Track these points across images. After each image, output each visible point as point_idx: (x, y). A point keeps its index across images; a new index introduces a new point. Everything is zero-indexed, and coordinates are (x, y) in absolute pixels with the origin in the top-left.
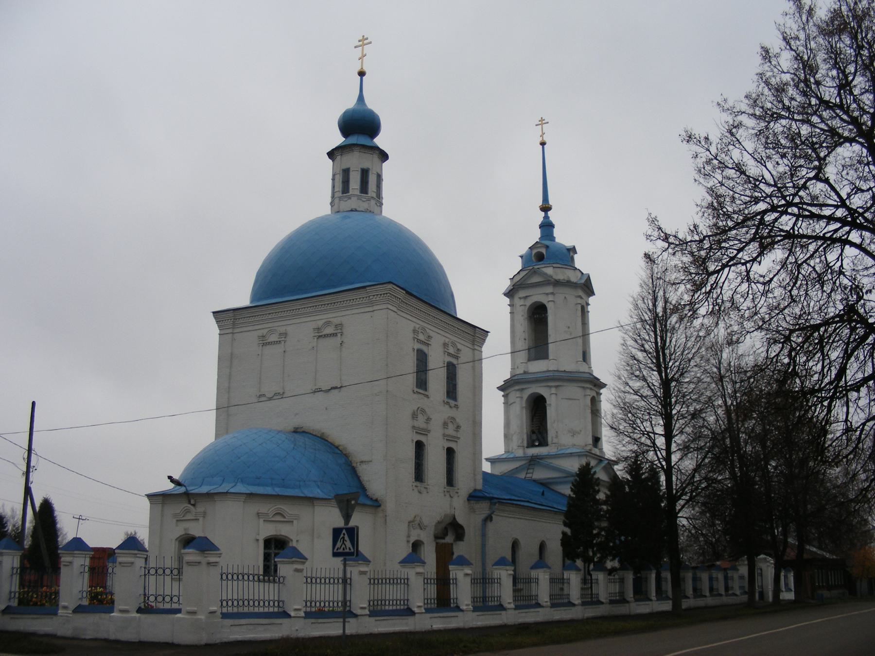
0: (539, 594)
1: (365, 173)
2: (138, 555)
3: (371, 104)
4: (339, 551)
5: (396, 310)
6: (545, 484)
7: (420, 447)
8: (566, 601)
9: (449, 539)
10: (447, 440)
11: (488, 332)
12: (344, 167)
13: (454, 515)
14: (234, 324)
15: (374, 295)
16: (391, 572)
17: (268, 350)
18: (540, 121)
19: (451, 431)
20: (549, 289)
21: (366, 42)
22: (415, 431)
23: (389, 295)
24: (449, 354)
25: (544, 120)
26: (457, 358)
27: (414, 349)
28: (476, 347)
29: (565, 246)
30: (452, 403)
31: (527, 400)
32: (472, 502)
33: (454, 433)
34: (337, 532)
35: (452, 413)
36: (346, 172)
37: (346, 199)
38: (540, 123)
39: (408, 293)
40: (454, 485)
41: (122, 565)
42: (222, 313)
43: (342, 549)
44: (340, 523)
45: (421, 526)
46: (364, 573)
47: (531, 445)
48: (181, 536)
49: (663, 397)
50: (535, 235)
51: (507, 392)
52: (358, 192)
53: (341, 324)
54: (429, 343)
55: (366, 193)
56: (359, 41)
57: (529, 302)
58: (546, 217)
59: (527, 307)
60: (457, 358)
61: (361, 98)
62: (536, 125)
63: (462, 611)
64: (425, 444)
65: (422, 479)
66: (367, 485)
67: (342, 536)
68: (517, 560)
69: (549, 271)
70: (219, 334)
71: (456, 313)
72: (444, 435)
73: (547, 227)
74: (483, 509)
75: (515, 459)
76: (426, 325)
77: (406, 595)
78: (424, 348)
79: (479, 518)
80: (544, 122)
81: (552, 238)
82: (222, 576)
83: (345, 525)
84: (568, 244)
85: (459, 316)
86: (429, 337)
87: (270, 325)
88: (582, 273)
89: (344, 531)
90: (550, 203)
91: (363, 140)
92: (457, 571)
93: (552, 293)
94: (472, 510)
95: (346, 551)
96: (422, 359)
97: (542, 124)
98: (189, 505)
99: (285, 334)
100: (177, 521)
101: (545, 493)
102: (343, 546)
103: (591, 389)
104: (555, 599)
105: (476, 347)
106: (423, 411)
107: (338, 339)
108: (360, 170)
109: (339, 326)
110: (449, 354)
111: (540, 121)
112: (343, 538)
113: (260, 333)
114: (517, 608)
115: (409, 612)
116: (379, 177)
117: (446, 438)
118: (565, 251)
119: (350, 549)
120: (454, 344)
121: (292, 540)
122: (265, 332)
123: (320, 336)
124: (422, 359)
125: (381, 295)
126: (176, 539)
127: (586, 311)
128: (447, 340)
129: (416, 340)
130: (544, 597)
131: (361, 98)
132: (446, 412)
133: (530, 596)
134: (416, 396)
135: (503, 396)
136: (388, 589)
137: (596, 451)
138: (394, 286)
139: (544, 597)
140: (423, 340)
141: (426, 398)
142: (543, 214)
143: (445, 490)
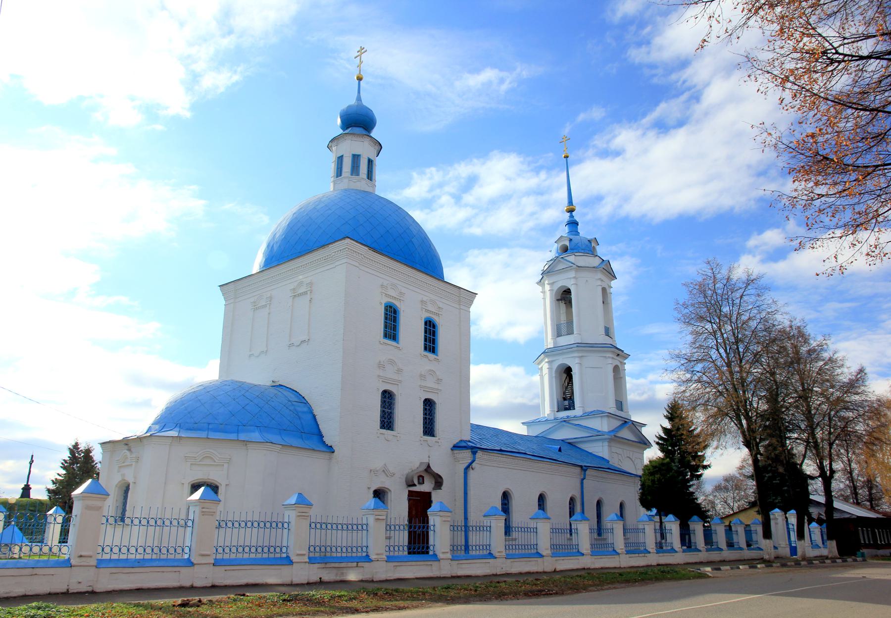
0: (491, 543)
3: (367, 102)
5: (357, 265)
8: (669, 548)
10: (382, 381)
11: (477, 294)
13: (429, 464)
15: (335, 252)
20: (572, 274)
21: (363, 51)
23: (347, 249)
24: (427, 311)
27: (381, 303)
28: (462, 307)
30: (431, 356)
31: (556, 371)
32: (456, 452)
33: (435, 386)
36: (340, 159)
40: (394, 429)
52: (348, 174)
55: (358, 174)
56: (358, 52)
58: (572, 216)
61: (359, 99)
65: (393, 427)
68: (624, 515)
69: (572, 258)
70: (225, 305)
71: (444, 279)
73: (573, 224)
77: (488, 540)
81: (577, 233)
88: (603, 260)
96: (391, 316)
100: (120, 467)
103: (613, 358)
105: (462, 307)
107: (308, 297)
108: (351, 156)
110: (427, 311)
113: (252, 300)
114: (628, 552)
115: (289, 561)
121: (390, 491)
128: (425, 299)
130: (620, 545)
131: (359, 99)
133: (601, 545)
139: (651, 545)
142: (569, 214)
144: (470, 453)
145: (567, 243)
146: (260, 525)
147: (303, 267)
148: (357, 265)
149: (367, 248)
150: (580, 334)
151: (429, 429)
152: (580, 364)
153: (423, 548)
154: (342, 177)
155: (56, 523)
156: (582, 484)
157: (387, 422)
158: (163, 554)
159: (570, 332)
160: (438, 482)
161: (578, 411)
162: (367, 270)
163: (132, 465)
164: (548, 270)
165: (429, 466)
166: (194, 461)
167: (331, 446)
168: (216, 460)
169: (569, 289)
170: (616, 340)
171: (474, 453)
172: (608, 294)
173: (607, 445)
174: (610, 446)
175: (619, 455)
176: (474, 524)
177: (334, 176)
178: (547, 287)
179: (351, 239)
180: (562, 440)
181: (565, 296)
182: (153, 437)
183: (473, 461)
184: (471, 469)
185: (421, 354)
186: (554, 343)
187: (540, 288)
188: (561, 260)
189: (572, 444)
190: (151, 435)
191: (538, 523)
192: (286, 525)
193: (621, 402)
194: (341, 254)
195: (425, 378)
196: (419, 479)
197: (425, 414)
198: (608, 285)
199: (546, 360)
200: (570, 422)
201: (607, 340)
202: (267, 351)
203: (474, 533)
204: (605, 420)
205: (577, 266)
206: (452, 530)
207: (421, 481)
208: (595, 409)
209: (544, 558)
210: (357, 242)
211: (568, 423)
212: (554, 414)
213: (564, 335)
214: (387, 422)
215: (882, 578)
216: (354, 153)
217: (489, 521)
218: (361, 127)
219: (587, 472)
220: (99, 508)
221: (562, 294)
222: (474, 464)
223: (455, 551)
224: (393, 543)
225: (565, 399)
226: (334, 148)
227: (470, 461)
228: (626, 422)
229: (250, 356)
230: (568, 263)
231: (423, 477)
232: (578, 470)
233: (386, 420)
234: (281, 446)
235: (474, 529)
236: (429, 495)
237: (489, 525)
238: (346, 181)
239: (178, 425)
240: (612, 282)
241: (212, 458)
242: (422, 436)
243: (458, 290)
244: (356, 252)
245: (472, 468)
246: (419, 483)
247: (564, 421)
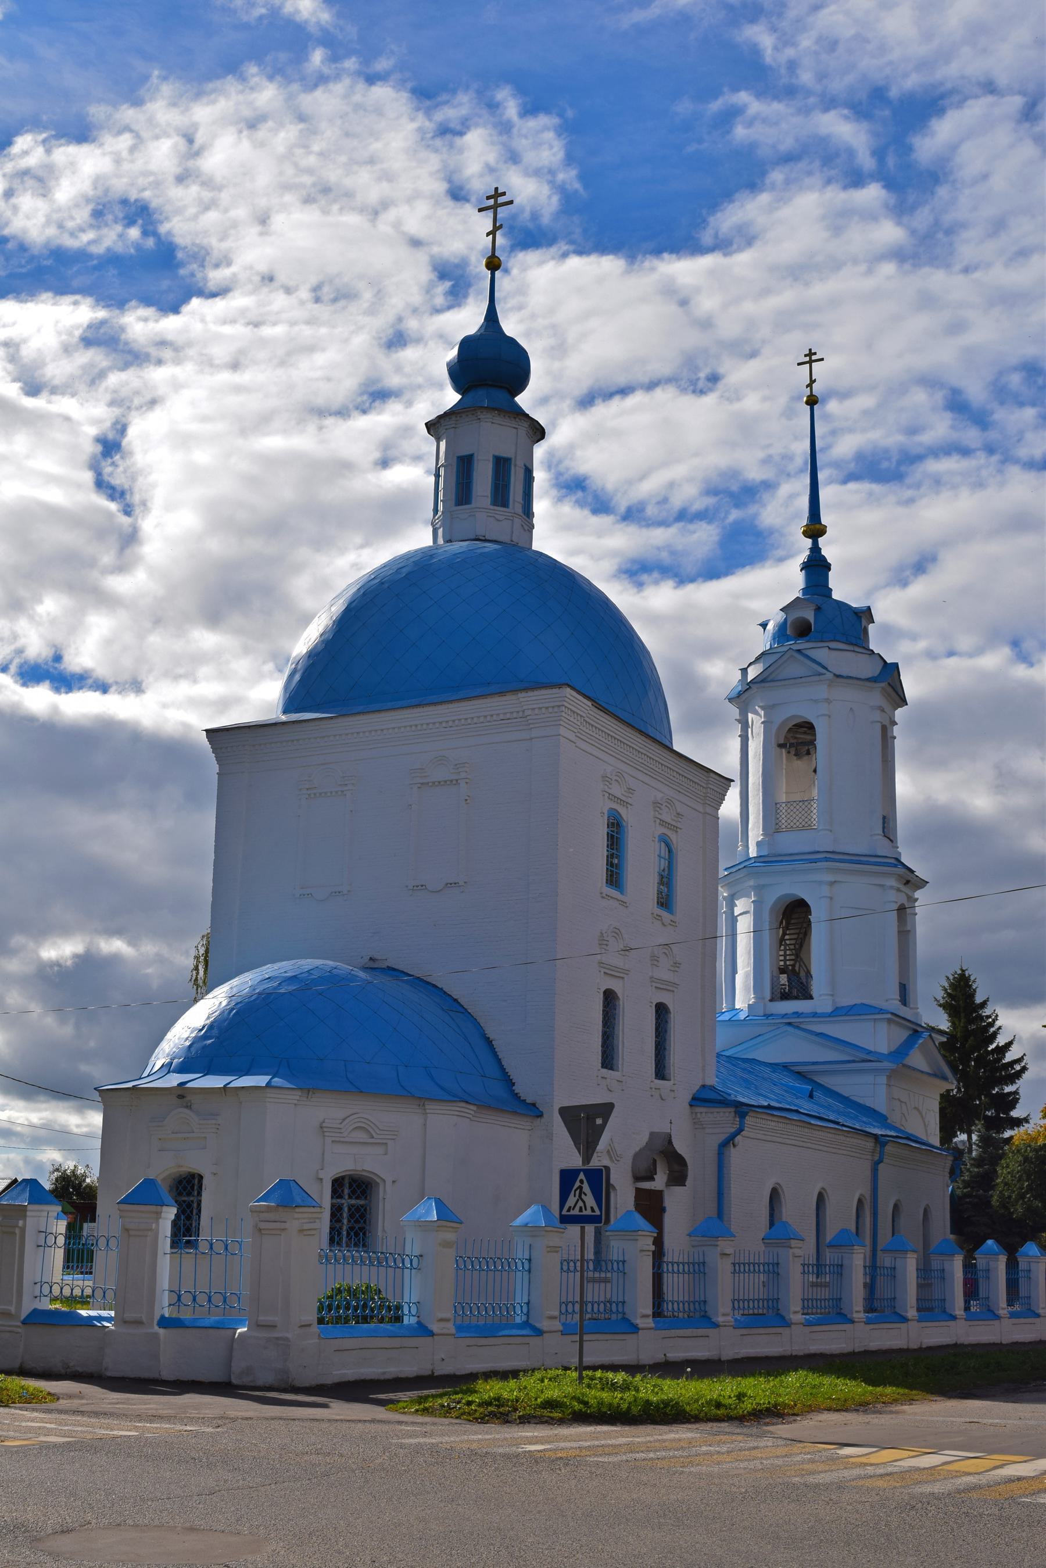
1: (501, 465)
4: (572, 1213)
9: (659, 1183)
12: (465, 451)
16: (742, 1252)
18: (806, 356)
20: (821, 691)
21: (501, 200)
22: (603, 970)
24: (663, 823)
25: (815, 354)
32: (698, 1110)
34: (568, 1178)
38: (807, 359)
40: (615, 1068)
43: (577, 1208)
44: (574, 1160)
46: (554, 1249)
52: (487, 501)
56: (488, 198)
58: (815, 549)
62: (799, 364)
63: (716, 1325)
67: (578, 1184)
69: (821, 654)
74: (723, 1120)
82: (562, 1264)
83: (584, 1164)
89: (582, 1176)
90: (823, 523)
91: (501, 395)
93: (828, 701)
94: (697, 1124)
95: (584, 1213)
97: (810, 362)
102: (580, 1204)
103: (898, 890)
111: (806, 356)
112: (580, 1188)
117: (654, 984)
119: (593, 1210)
127: (889, 735)
136: (882, 1280)
137: (904, 1012)
140: (619, 795)
142: (809, 542)
144: (733, 1114)
147: (444, 725)
149: (589, 703)
152: (831, 898)
154: (472, 506)
155: (213, 1253)
156: (875, 1171)
158: (185, 1305)
161: (821, 999)
166: (338, 1135)
167: (534, 1105)
168: (374, 1134)
170: (899, 845)
171: (742, 1115)
172: (889, 739)
173: (885, 1082)
174: (890, 1086)
175: (903, 1105)
183: (740, 1131)
184: (732, 1145)
185: (653, 914)
189: (804, 1077)
191: (897, 1259)
193: (905, 985)
195: (658, 961)
198: (890, 719)
199: (752, 883)
200: (801, 1026)
201: (882, 848)
204: (883, 1027)
205: (835, 675)
208: (858, 1001)
209: (909, 1322)
210: (579, 692)
211: (798, 1027)
216: (497, 454)
218: (501, 387)
219: (749, 1120)
221: (790, 730)
222: (738, 1138)
223: (596, 1302)
227: (733, 1130)
228: (916, 1031)
232: (870, 1144)
236: (660, 1193)
240: (896, 712)
241: (369, 1131)
242: (600, 1068)
243: (706, 774)
245: (733, 1144)
247: (789, 1024)
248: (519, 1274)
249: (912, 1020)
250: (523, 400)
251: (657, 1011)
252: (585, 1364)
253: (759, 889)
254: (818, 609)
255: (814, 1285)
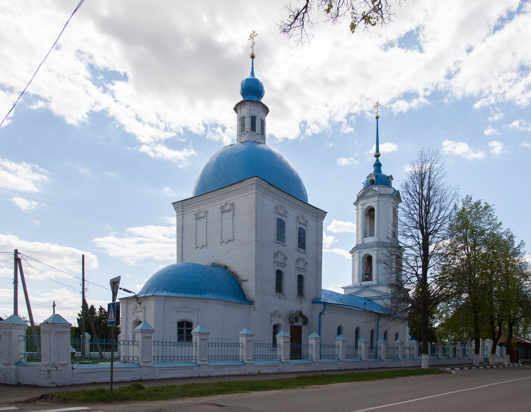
1: (253, 119)
2: (13, 328)
5: (262, 194)
6: (369, 300)
7: (279, 274)
14: (183, 209)
17: (199, 221)
19: (301, 265)
20: (376, 199)
22: (276, 264)
24: (300, 223)
26: (305, 225)
27: (275, 218)
28: (319, 221)
29: (386, 176)
30: (302, 250)
32: (314, 304)
35: (303, 256)
37: (243, 135)
38: (376, 105)
39: (269, 183)
41: (45, 332)
42: (176, 203)
45: (280, 316)
47: (367, 280)
48: (135, 321)
49: (422, 244)
50: (372, 170)
51: (353, 254)
53: (233, 204)
54: (286, 215)
57: (365, 207)
58: (378, 160)
59: (364, 209)
60: (305, 225)
64: (283, 271)
66: (246, 293)
69: (376, 188)
71: (308, 202)
72: (296, 268)
73: (378, 165)
75: (356, 287)
76: (283, 205)
78: (283, 218)
79: (317, 313)
80: (378, 104)
81: (381, 172)
84: (388, 175)
85: (309, 203)
86: (286, 212)
87: (199, 208)
88: (395, 190)
91: (255, 99)
92: (280, 340)
96: (281, 225)
98: (138, 304)
99: (207, 212)
100: (133, 312)
101: (366, 303)
104: (371, 355)
105: (319, 221)
106: (282, 253)
108: (250, 117)
109: (233, 205)
110: (300, 223)
113: (194, 213)
116: (263, 123)
118: (386, 178)
120: (303, 217)
121: (281, 325)
122: (197, 212)
123: (223, 212)
124: (281, 225)
125: (252, 184)
126: (133, 322)
128: (299, 215)
129: (277, 213)
132: (298, 255)
133: (332, 355)
134: (277, 245)
135: (352, 256)
138: (259, 179)
141: (284, 247)
142: (376, 159)
143: (297, 297)
145: (374, 178)
146: (157, 343)
148: (261, 194)
150: (378, 236)
151: (300, 292)
153: (298, 356)
157: (279, 288)
159: (372, 235)
160: (306, 320)
161: (374, 282)
162: (267, 197)
163: (142, 311)
164: (361, 195)
165: (301, 312)
169: (374, 208)
176: (168, 340)
177: (239, 131)
178: (360, 207)
179: (258, 177)
180: (364, 298)
181: (370, 213)
182: (154, 296)
183: (324, 310)
186: (363, 241)
187: (355, 207)
188: (370, 189)
190: (153, 295)
192: (241, 345)
194: (252, 186)
196: (295, 319)
197: (298, 283)
202: (207, 245)
203: (324, 348)
206: (254, 346)
207: (297, 320)
212: (360, 283)
213: (368, 237)
214: (279, 288)
215: (325, 386)
217: (338, 343)
220: (150, 337)
221: (369, 211)
222: (324, 312)
224: (169, 354)
225: (366, 274)
226: (239, 111)
229: (196, 248)
230: (374, 192)
231: (298, 318)
233: (278, 287)
234: (225, 302)
235: (328, 347)
236: (300, 327)
237: (338, 344)
238: (248, 135)
239: (166, 289)
244: (261, 186)
246: (296, 322)
248: (336, 348)
249: (182, 221)
250: (263, 101)
251: (298, 278)
252: (114, 381)
253: (360, 253)
254: (376, 176)
255: (370, 352)
